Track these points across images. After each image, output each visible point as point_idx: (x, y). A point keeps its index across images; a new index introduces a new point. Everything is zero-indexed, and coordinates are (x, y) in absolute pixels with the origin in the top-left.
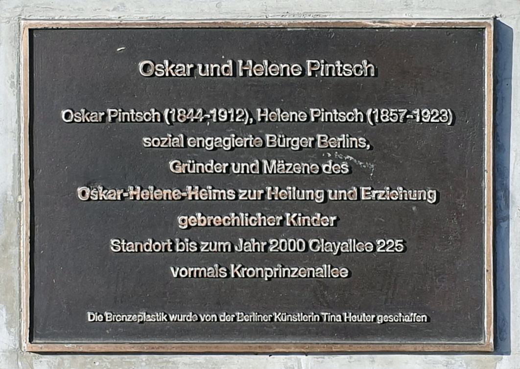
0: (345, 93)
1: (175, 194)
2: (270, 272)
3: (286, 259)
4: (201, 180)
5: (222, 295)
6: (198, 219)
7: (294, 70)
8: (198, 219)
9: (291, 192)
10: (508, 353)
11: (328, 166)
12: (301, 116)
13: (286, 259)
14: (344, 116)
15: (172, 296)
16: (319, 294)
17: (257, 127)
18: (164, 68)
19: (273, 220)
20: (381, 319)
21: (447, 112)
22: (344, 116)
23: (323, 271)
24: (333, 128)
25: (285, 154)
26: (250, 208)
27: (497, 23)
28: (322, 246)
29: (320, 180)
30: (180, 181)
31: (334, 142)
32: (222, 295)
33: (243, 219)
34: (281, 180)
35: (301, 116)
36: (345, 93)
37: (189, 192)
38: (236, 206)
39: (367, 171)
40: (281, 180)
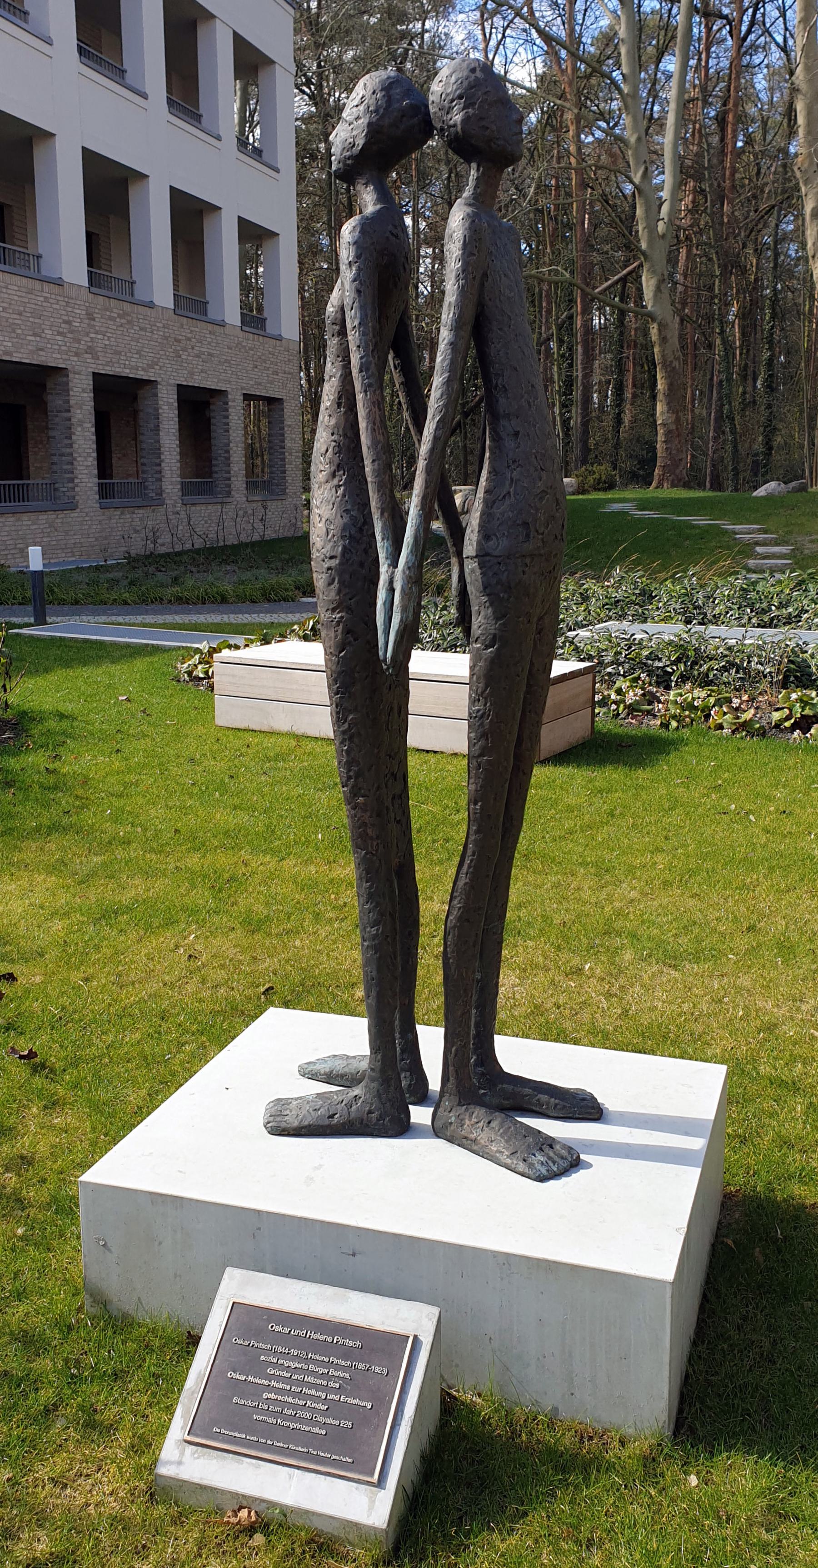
0: (347, 1353)
1: (266, 1383)
2: (292, 1425)
3: (302, 1420)
4: (279, 1379)
5: (271, 1431)
6: (272, 1396)
7: (329, 1339)
8: (272, 1396)
9: (313, 1392)
10: (72, 506)
11: (331, 1384)
12: (326, 1360)
13: (302, 1420)
14: (343, 1363)
15: (251, 1427)
16: (310, 1439)
17: (307, 1360)
18: (278, 1328)
19: (302, 1403)
20: (333, 1457)
21: (403, 1075)
22: (343, 1363)
23: (316, 1430)
24: (338, 1367)
25: (313, 1373)
26: (295, 1395)
27: (416, 1337)
28: (321, 1419)
29: (326, 1389)
30: (270, 1377)
31: (337, 1374)
32: (271, 1431)
33: (290, 1400)
34: (311, 1386)
35: (326, 1360)
36: (347, 1353)
37: (273, 1383)
38: (289, 1392)
39: (346, 1389)
40: (311, 1386)
